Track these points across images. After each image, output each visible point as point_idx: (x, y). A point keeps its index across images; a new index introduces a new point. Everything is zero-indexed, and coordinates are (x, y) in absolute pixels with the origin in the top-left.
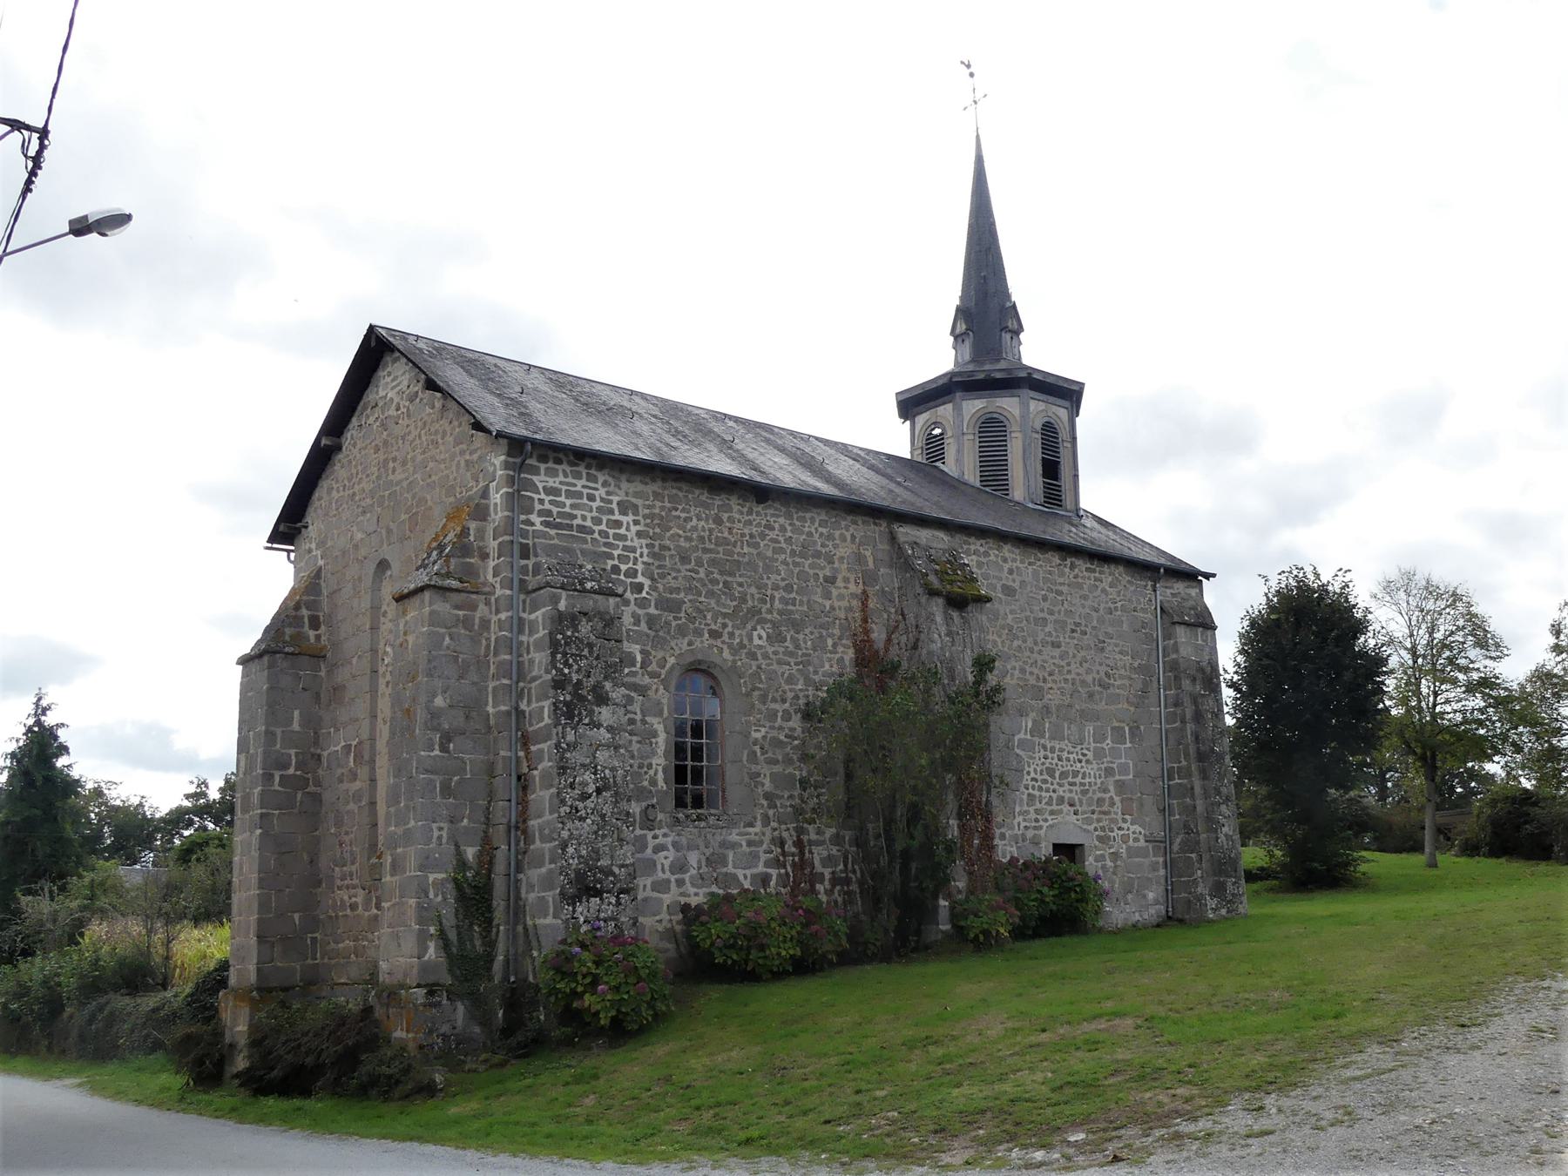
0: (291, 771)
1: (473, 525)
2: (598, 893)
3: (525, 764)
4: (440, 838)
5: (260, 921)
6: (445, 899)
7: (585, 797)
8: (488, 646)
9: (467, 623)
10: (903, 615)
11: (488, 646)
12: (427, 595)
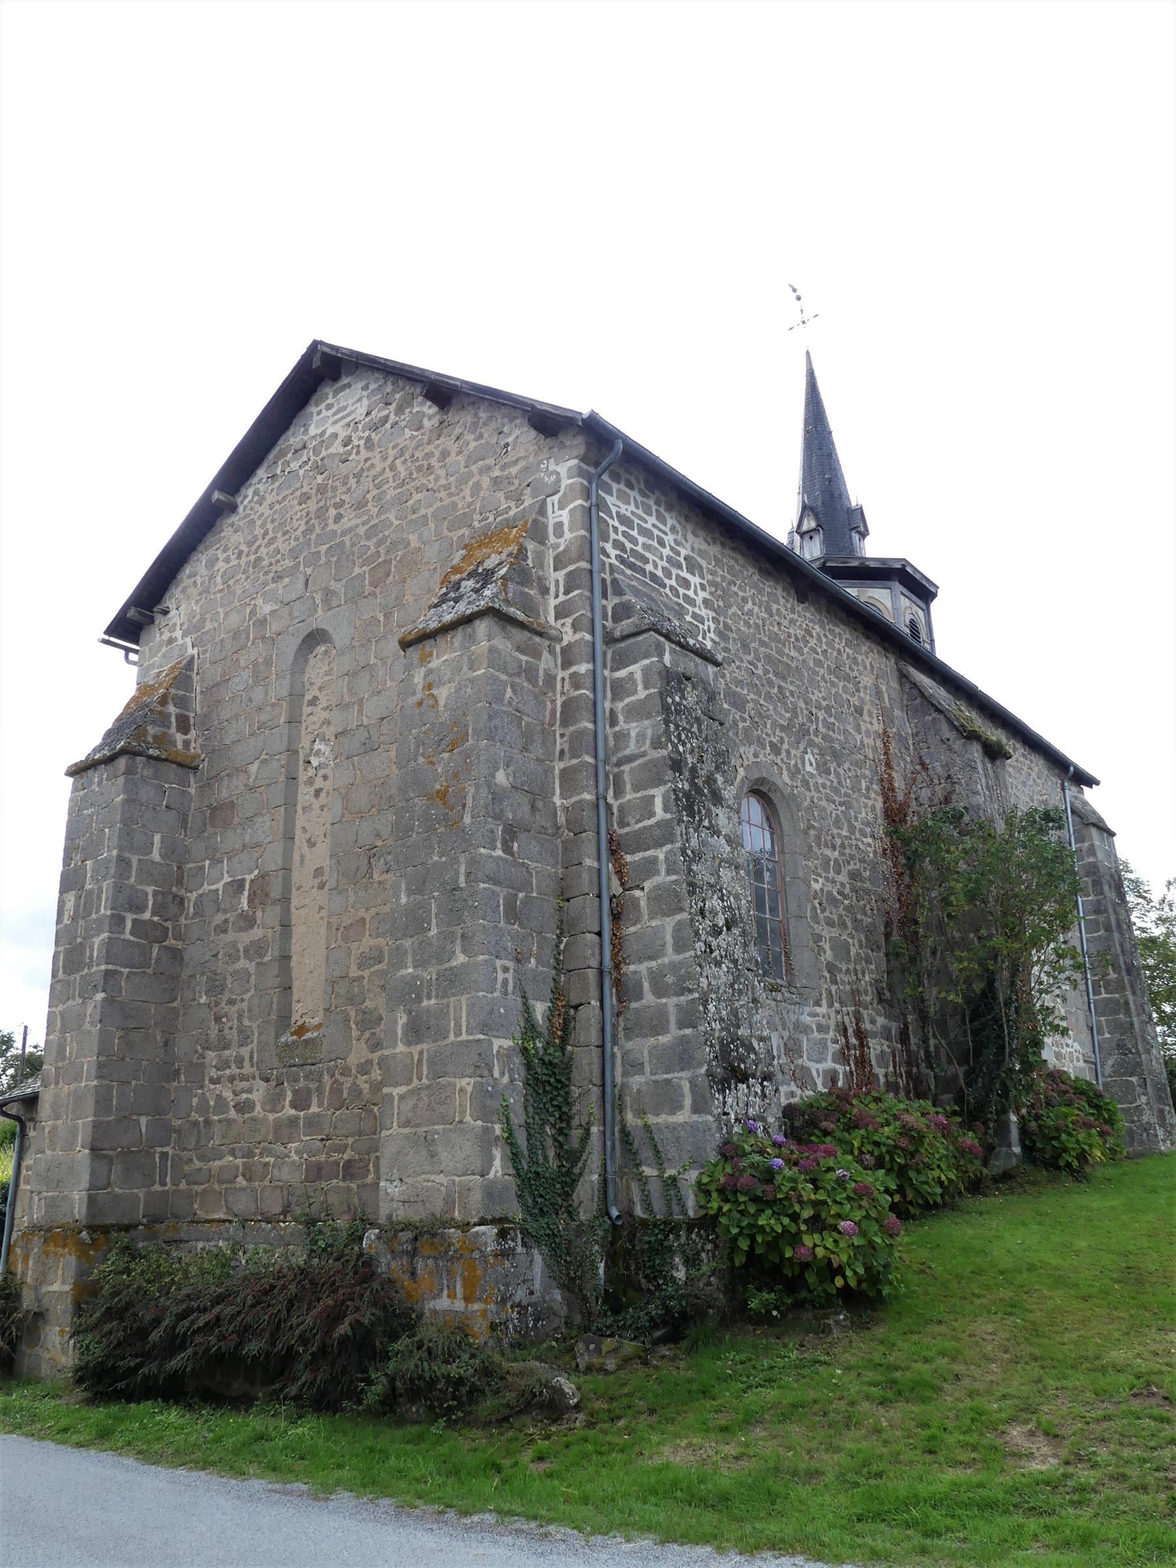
0: (147, 915)
1: (531, 546)
2: (744, 1078)
3: (615, 882)
4: (505, 983)
5: (96, 1126)
6: (512, 1080)
7: (716, 932)
8: (553, 712)
9: (530, 673)
10: (923, 764)
11: (553, 712)
12: (482, 627)
